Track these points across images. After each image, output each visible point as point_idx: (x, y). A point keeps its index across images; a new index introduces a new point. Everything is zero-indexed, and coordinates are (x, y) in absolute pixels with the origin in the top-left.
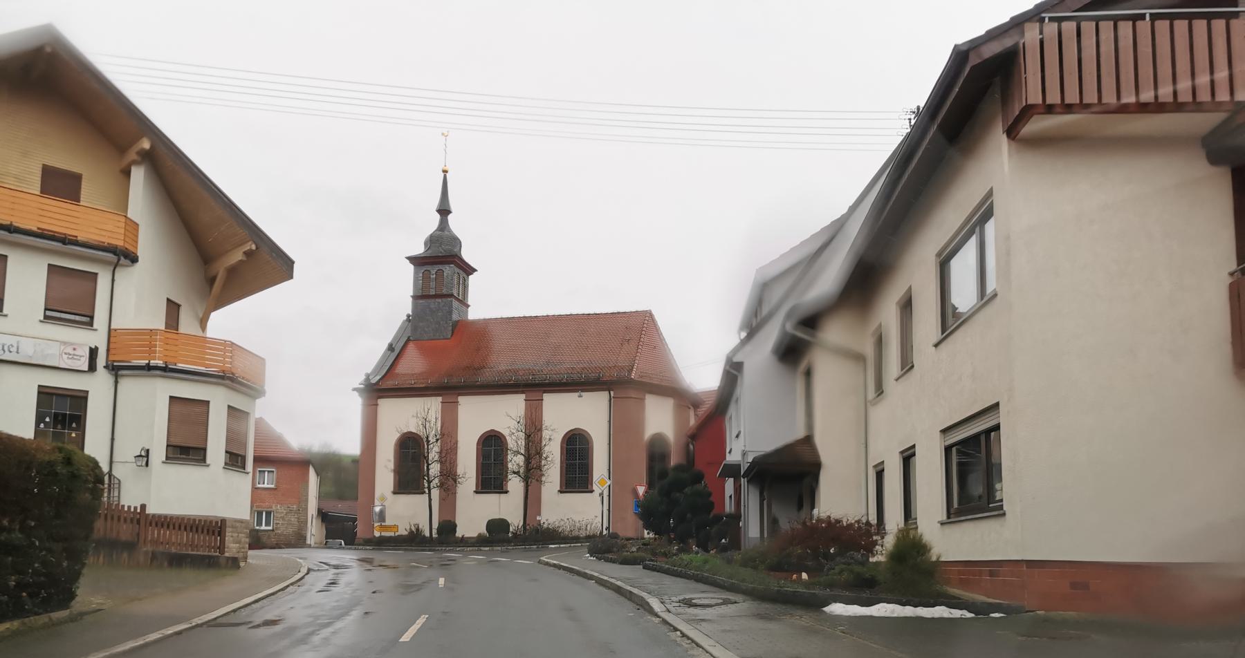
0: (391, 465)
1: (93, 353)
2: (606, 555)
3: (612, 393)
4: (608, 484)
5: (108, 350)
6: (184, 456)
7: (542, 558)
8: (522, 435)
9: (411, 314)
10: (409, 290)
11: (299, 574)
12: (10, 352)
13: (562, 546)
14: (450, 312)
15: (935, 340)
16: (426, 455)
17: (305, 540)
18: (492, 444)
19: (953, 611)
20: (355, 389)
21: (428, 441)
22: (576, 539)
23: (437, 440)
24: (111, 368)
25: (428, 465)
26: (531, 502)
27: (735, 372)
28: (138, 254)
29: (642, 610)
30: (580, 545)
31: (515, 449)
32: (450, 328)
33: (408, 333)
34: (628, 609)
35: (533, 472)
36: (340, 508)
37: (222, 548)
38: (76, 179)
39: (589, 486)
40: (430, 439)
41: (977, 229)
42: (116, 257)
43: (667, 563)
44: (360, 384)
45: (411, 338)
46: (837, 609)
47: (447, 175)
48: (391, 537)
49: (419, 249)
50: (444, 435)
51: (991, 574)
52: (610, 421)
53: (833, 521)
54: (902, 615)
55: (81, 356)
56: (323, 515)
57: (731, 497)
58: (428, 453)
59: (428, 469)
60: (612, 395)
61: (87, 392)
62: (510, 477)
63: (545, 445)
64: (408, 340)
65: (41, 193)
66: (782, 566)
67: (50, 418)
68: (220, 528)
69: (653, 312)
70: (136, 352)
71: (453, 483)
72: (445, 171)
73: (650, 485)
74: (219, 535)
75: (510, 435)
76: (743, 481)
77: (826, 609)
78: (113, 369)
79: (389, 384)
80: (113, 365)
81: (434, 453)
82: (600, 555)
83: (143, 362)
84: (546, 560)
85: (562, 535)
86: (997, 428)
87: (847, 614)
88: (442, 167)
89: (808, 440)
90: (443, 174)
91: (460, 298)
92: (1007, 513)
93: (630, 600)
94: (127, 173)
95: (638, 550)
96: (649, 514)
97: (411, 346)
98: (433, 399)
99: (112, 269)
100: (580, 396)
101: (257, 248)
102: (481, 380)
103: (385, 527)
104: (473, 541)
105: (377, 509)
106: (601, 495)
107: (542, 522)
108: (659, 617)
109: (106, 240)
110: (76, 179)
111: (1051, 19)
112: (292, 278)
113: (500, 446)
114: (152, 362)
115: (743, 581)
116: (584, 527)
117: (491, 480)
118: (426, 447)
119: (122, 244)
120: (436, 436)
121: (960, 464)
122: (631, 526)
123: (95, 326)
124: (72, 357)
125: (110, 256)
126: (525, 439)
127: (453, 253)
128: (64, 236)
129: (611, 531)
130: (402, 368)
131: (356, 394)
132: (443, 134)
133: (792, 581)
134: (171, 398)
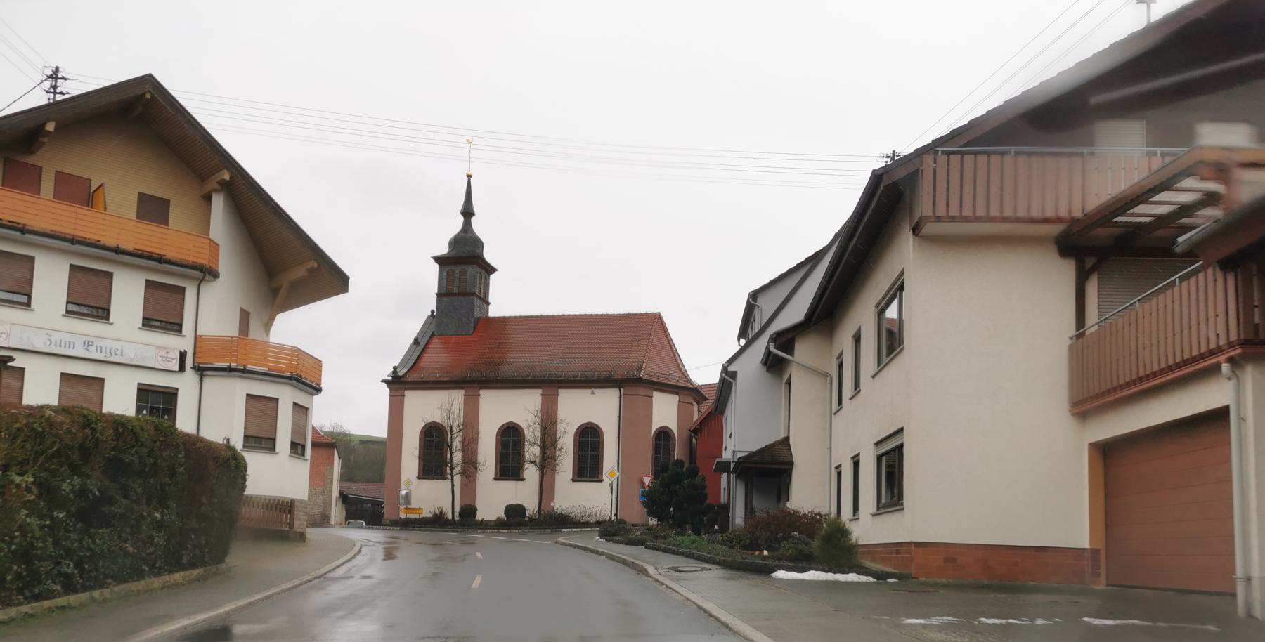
0: (417, 453)
1: (183, 356)
2: (615, 538)
3: (622, 390)
4: (616, 476)
5: (194, 354)
6: (257, 445)
7: (558, 539)
8: (538, 428)
9: (435, 310)
10: (434, 288)
11: (356, 547)
12: (116, 355)
13: (573, 530)
14: (473, 310)
15: (872, 373)
16: (450, 444)
17: (330, 520)
18: (510, 436)
19: (861, 577)
20: (383, 381)
21: (452, 431)
22: (587, 524)
23: (460, 431)
24: (197, 369)
25: (451, 453)
26: (546, 489)
27: (730, 380)
28: (219, 271)
29: (641, 574)
30: (590, 529)
31: (532, 440)
32: (473, 325)
33: (433, 328)
34: (630, 574)
35: (548, 462)
36: (358, 490)
37: (291, 525)
38: (166, 203)
39: (599, 476)
40: (454, 429)
41: (898, 294)
42: (202, 274)
43: (664, 543)
44: (388, 376)
45: (435, 333)
46: (781, 574)
47: (472, 179)
48: (416, 519)
49: (444, 250)
50: (466, 426)
51: (898, 552)
52: (619, 438)
53: (792, 512)
54: (825, 579)
55: (173, 359)
56: (344, 497)
57: (725, 489)
58: (452, 442)
59: (451, 458)
60: (622, 392)
61: (177, 389)
62: (527, 466)
63: (559, 438)
64: (433, 335)
65: (137, 218)
66: (753, 546)
67: (147, 411)
68: (290, 506)
69: (662, 315)
70: (216, 356)
71: (474, 470)
72: (469, 176)
73: (656, 475)
74: (289, 513)
75: (528, 428)
76: (733, 476)
77: (773, 575)
78: (199, 370)
79: (414, 377)
80: (199, 367)
81: (457, 443)
82: (609, 537)
83: (225, 365)
84: (562, 541)
85: (574, 520)
86: (901, 447)
87: (787, 578)
88: (466, 172)
89: (786, 440)
90: (467, 179)
91: (482, 296)
92: (905, 510)
93: (633, 568)
94: (208, 198)
95: (641, 534)
96: (653, 502)
97: (435, 340)
98: (457, 391)
99: (198, 283)
100: (593, 393)
101: (319, 265)
102: (501, 375)
103: (411, 509)
104: (493, 524)
105: (403, 493)
106: (611, 485)
107: (555, 508)
108: (653, 578)
109: (191, 258)
110: (166, 203)
111: (943, 152)
112: (347, 291)
113: (518, 437)
114: (232, 364)
115: (718, 555)
116: (594, 513)
117: (509, 468)
118: (449, 436)
119: (207, 263)
120: (459, 426)
121: (888, 466)
122: (636, 513)
123: (184, 333)
124: (166, 359)
125: (197, 273)
126: (541, 431)
127: (476, 255)
128: (159, 256)
129: (618, 518)
130: (424, 363)
131: (384, 384)
132: (467, 140)
133: (756, 556)
134: (248, 395)
